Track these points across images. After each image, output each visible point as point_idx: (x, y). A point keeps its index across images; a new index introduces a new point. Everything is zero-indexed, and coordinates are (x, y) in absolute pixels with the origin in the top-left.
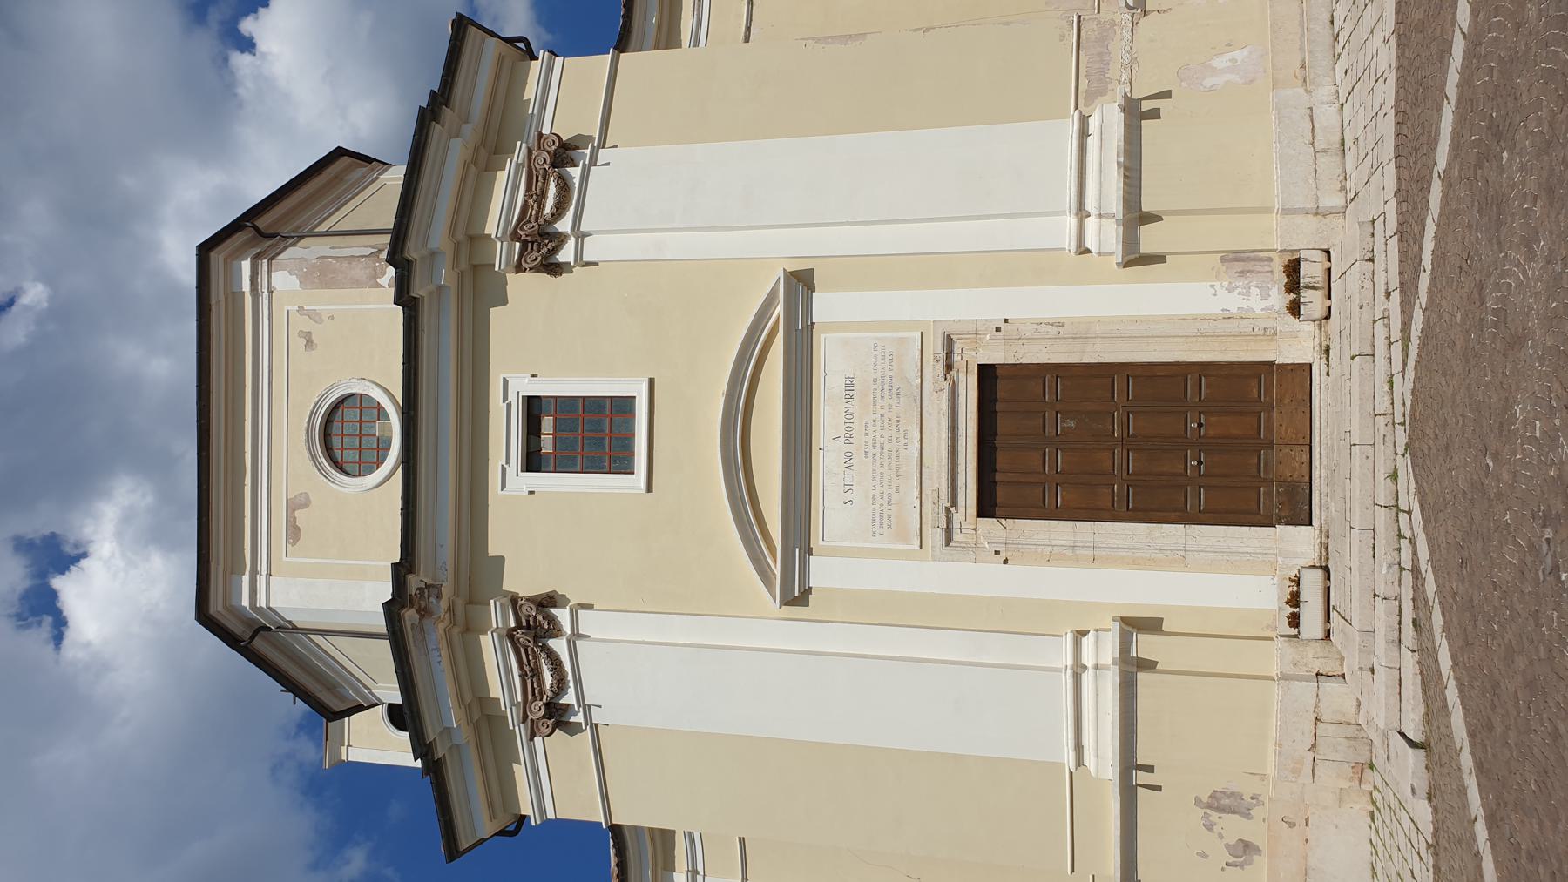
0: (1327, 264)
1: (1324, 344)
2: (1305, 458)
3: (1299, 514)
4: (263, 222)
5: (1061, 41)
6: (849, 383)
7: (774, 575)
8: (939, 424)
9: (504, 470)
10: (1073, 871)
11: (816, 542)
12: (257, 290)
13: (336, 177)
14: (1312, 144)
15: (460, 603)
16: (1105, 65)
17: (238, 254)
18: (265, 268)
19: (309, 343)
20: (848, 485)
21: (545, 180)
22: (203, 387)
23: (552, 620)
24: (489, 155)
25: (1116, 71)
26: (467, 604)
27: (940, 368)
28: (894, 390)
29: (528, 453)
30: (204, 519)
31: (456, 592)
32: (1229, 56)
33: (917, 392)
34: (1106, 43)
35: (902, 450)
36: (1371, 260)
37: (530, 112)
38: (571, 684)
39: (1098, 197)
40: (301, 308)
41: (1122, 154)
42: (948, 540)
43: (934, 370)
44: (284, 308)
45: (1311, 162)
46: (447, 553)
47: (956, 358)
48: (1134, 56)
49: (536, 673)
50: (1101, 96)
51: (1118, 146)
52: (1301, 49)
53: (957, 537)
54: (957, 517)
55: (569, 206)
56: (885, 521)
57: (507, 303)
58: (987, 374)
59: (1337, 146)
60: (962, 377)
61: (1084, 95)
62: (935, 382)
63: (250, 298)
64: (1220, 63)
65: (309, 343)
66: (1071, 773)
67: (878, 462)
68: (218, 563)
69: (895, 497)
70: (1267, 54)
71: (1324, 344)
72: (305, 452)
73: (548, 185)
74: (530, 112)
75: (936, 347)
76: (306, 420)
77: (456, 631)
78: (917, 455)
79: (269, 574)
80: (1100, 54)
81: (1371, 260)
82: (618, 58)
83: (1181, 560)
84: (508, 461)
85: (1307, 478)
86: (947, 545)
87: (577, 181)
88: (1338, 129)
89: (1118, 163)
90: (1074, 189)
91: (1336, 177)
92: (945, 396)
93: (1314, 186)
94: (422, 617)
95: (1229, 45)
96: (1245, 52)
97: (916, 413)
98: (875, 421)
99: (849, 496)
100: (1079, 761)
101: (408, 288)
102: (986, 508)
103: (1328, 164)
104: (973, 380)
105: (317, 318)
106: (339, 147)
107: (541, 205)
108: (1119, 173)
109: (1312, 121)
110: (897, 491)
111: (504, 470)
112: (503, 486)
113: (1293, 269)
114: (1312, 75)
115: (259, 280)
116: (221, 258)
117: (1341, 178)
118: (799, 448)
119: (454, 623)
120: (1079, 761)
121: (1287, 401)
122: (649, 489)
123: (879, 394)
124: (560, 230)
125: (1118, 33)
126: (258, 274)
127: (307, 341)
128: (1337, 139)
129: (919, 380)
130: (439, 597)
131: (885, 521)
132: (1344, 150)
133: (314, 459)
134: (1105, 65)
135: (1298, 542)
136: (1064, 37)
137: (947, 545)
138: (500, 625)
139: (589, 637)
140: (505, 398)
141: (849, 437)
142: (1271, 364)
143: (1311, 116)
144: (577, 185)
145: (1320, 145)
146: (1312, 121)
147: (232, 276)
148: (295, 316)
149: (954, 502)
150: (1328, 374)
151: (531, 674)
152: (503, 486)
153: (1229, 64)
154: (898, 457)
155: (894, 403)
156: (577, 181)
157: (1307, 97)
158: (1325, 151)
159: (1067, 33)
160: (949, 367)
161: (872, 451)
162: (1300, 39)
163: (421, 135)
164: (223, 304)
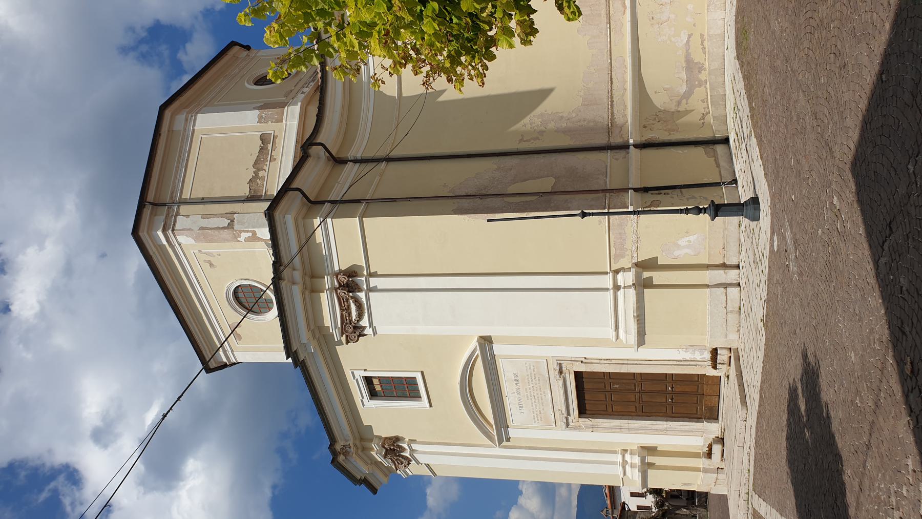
0: (730, 355)
1: (727, 374)
2: (717, 399)
3: (712, 415)
4: (151, 197)
5: (599, 224)
6: (516, 376)
7: (494, 436)
8: (559, 390)
9: (362, 401)
10: (623, 485)
11: (510, 423)
12: (172, 244)
13: (169, 131)
14: (726, 308)
15: (358, 443)
16: (623, 240)
17: (151, 228)
18: (172, 234)
19: (211, 265)
20: (521, 407)
21: (347, 303)
22: (172, 304)
23: (400, 447)
24: (313, 291)
25: (629, 245)
26: (311, 293)
27: (557, 373)
28: (537, 378)
29: (370, 391)
30: (192, 339)
31: (355, 439)
32: (687, 239)
33: (547, 379)
34: (623, 227)
35: (543, 397)
36: (746, 421)
37: (324, 254)
38: (366, 311)
39: (625, 326)
40: (200, 251)
41: (635, 311)
42: (567, 424)
43: (554, 374)
44: (190, 253)
45: (724, 317)
46: (347, 431)
47: (564, 369)
48: (639, 236)
49: (348, 309)
50: (622, 258)
51: (633, 307)
52: (723, 237)
53: (571, 424)
54: (570, 418)
55: (365, 313)
56: (539, 419)
57: (371, 426)
58: (578, 375)
59: (737, 309)
60: (567, 375)
61: (614, 257)
62: (555, 377)
63: (170, 249)
64: (683, 242)
65: (211, 265)
66: (622, 479)
67: (533, 401)
68: (166, 274)
69: (542, 412)
70: (706, 238)
71: (727, 374)
72: (229, 307)
73: (350, 302)
74: (324, 254)
75: (554, 366)
76: (225, 296)
77: (359, 452)
78: (550, 399)
79: (232, 351)
80: (620, 234)
81: (746, 421)
82: (362, 221)
83: (665, 432)
84: (363, 397)
85: (717, 405)
86: (567, 427)
87: (364, 300)
88: (738, 303)
89: (634, 316)
90: (613, 323)
91: (735, 325)
92: (561, 382)
93: (726, 329)
94: (345, 456)
95: (687, 232)
96: (695, 237)
97: (548, 386)
98: (530, 388)
99: (522, 411)
100: (625, 474)
101: (298, 358)
102: (582, 412)
103: (732, 318)
104: (573, 376)
105: (211, 255)
106: (160, 107)
107: (350, 315)
108: (634, 321)
109: (726, 295)
110: (543, 410)
111: (362, 401)
112: (363, 405)
113: (714, 352)
114: (728, 256)
115: (171, 240)
116: (145, 233)
117: (738, 325)
118: (500, 416)
119: (357, 448)
120: (625, 474)
121: (710, 382)
122: (431, 406)
123: (530, 380)
124: (363, 325)
125: (630, 222)
126: (168, 237)
127: (210, 264)
128: (737, 306)
129: (548, 376)
130: (350, 448)
131: (539, 419)
132: (740, 312)
133: (236, 310)
134: (623, 240)
135: (712, 429)
136: (601, 222)
137: (567, 427)
138: (378, 449)
139: (416, 440)
140: (354, 378)
141: (519, 393)
142: (704, 375)
143: (726, 293)
144: (365, 302)
145: (729, 309)
146: (726, 295)
147: (156, 240)
148: (198, 254)
149: (569, 414)
150: (728, 383)
151: (346, 310)
152: (363, 405)
153: (687, 243)
154: (542, 399)
155: (537, 382)
156: (364, 300)
157: (725, 275)
158: (731, 312)
159: (602, 221)
160: (561, 373)
161: (530, 398)
162: (723, 232)
163: (278, 295)
164: (156, 252)
